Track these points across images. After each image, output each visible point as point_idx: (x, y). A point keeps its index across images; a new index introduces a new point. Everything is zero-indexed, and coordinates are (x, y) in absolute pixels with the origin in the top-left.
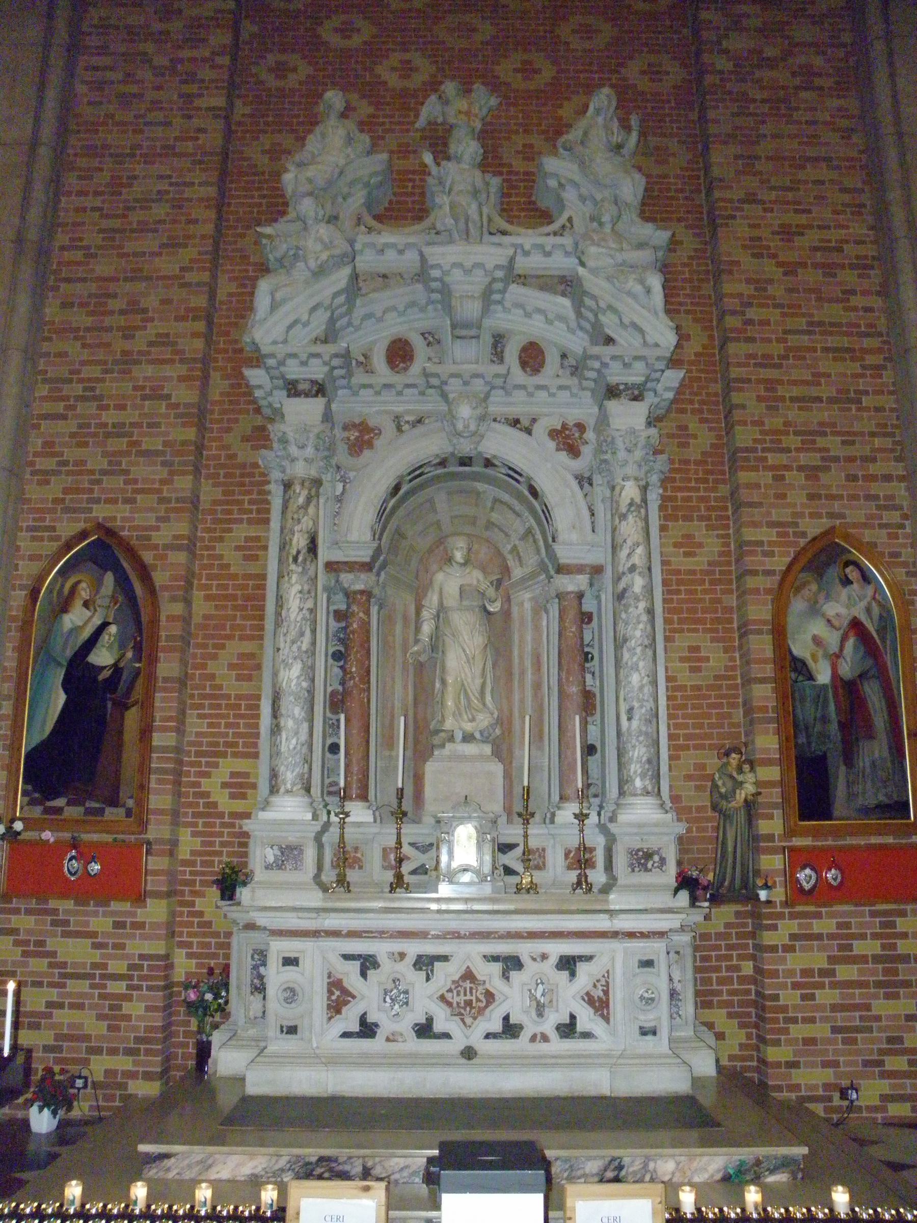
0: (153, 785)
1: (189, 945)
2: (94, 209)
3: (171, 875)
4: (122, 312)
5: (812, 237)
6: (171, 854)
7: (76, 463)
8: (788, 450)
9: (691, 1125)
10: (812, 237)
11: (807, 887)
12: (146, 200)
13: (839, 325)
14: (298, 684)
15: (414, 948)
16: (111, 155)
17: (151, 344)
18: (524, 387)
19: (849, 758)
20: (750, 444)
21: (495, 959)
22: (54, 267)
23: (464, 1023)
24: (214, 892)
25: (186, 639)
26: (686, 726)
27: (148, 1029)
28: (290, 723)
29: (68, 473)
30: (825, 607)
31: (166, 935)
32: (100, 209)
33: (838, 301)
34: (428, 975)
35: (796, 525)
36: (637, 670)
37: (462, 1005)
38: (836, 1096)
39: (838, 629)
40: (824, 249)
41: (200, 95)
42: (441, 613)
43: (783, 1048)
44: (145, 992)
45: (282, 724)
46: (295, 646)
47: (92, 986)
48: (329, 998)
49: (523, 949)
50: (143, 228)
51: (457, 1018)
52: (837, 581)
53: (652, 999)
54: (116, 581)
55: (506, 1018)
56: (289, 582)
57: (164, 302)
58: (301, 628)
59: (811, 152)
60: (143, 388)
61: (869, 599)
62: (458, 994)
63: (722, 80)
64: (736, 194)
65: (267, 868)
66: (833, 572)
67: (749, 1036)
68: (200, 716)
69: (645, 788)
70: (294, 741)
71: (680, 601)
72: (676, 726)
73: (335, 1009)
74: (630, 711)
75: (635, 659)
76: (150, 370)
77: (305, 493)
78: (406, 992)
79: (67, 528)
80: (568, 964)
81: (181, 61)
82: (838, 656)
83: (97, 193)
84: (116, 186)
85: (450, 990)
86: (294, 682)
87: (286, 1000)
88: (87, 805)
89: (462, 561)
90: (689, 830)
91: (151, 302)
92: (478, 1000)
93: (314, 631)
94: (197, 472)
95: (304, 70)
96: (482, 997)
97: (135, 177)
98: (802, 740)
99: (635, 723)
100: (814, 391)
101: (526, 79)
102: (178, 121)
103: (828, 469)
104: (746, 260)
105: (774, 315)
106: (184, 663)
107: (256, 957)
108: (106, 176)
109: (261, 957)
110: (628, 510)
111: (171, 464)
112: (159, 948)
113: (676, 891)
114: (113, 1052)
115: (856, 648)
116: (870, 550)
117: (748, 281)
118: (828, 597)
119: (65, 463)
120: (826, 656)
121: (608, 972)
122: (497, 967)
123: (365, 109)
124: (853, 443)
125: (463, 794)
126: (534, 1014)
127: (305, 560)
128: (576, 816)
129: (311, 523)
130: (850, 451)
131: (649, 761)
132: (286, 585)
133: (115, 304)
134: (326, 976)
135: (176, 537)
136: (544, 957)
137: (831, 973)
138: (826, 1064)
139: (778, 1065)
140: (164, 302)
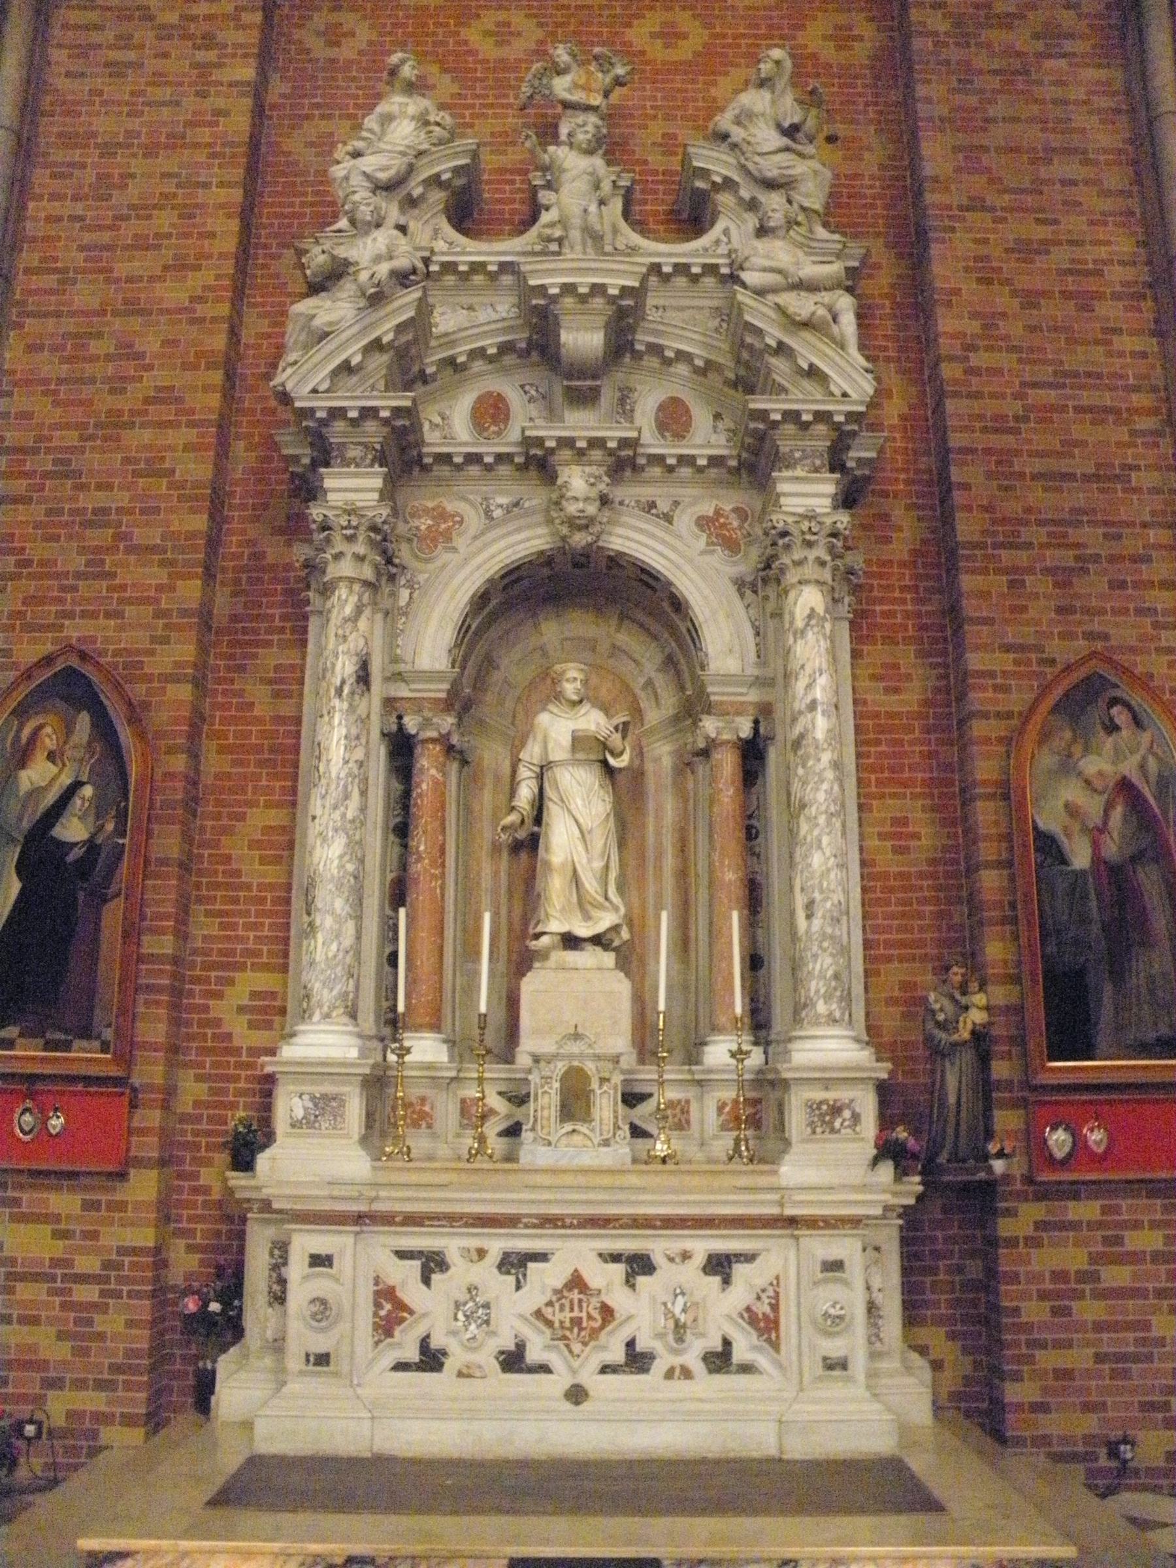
0: (141, 1009)
1: (190, 1233)
2: (73, 218)
3: (166, 1137)
4: (108, 358)
5: (1060, 256)
6: (166, 1106)
7: (42, 563)
8: (1029, 545)
9: (899, 1508)
10: (1060, 256)
11: (1059, 1154)
12: (145, 207)
13: (1099, 376)
14: (341, 867)
15: (498, 1244)
16: (97, 145)
17: (147, 401)
18: (659, 459)
19: (1118, 975)
20: (976, 538)
21: (615, 1258)
22: (17, 297)
23: (571, 1351)
24: (222, 1158)
25: (192, 803)
26: (887, 929)
27: (131, 1353)
28: (329, 922)
29: (30, 576)
30: (1081, 763)
31: (158, 1220)
32: (81, 219)
33: (1097, 342)
34: (518, 1281)
35: (1040, 649)
36: (820, 847)
37: (568, 1324)
38: (1103, 1452)
39: (1101, 793)
40: (1078, 272)
41: (220, 65)
42: (543, 771)
43: (1027, 1383)
44: (125, 1300)
45: (318, 922)
46: (338, 812)
47: (53, 1292)
48: (375, 1314)
49: (658, 1246)
50: (142, 245)
51: (561, 1344)
52: (1099, 727)
53: (841, 1318)
54: (94, 725)
55: (631, 1344)
56: (330, 723)
57: (166, 343)
58: (345, 787)
59: (1056, 141)
60: (137, 461)
61: (1142, 751)
62: (562, 1309)
63: (936, 44)
64: (956, 199)
65: (293, 1126)
66: (1095, 714)
67: (977, 1365)
68: (208, 913)
69: (831, 1014)
70: (334, 947)
71: (881, 755)
72: (876, 929)
73: (386, 1328)
74: (810, 906)
75: (816, 832)
76: (147, 435)
77: (354, 599)
78: (487, 1306)
79: (29, 651)
80: (720, 1265)
81: (194, 18)
82: (1102, 829)
83: (76, 198)
84: (104, 186)
85: (550, 1304)
86: (336, 862)
87: (314, 1316)
88: (48, 1035)
89: (575, 698)
90: (892, 1073)
91: (150, 344)
92: (590, 1317)
93: (364, 793)
94: (209, 575)
95: (364, 34)
96: (596, 1314)
97: (132, 176)
98: (1051, 949)
99: (817, 923)
100: (1064, 466)
101: (667, 46)
102: (190, 102)
103: (1086, 571)
104: (969, 287)
105: (1005, 360)
106: (187, 838)
107: (276, 1252)
108: (90, 176)
109: (281, 1249)
110: (807, 625)
111: (172, 563)
112: (146, 1237)
113: (875, 1161)
114: (80, 1384)
115: (1125, 819)
116: (1145, 682)
117: (974, 315)
118: (1087, 750)
119: (28, 563)
120: (1085, 830)
121: (777, 1278)
122: (619, 1269)
123: (446, 86)
124: (1119, 537)
125: (573, 1023)
126: (671, 1338)
127: (352, 693)
128: (733, 1055)
129: (362, 642)
130: (1115, 548)
131: (836, 976)
132: (326, 728)
133: (97, 347)
134: (371, 1282)
135: (177, 664)
136: (686, 1256)
137: (1095, 1277)
138: (1087, 1407)
139: (1019, 1407)
140: (166, 343)
